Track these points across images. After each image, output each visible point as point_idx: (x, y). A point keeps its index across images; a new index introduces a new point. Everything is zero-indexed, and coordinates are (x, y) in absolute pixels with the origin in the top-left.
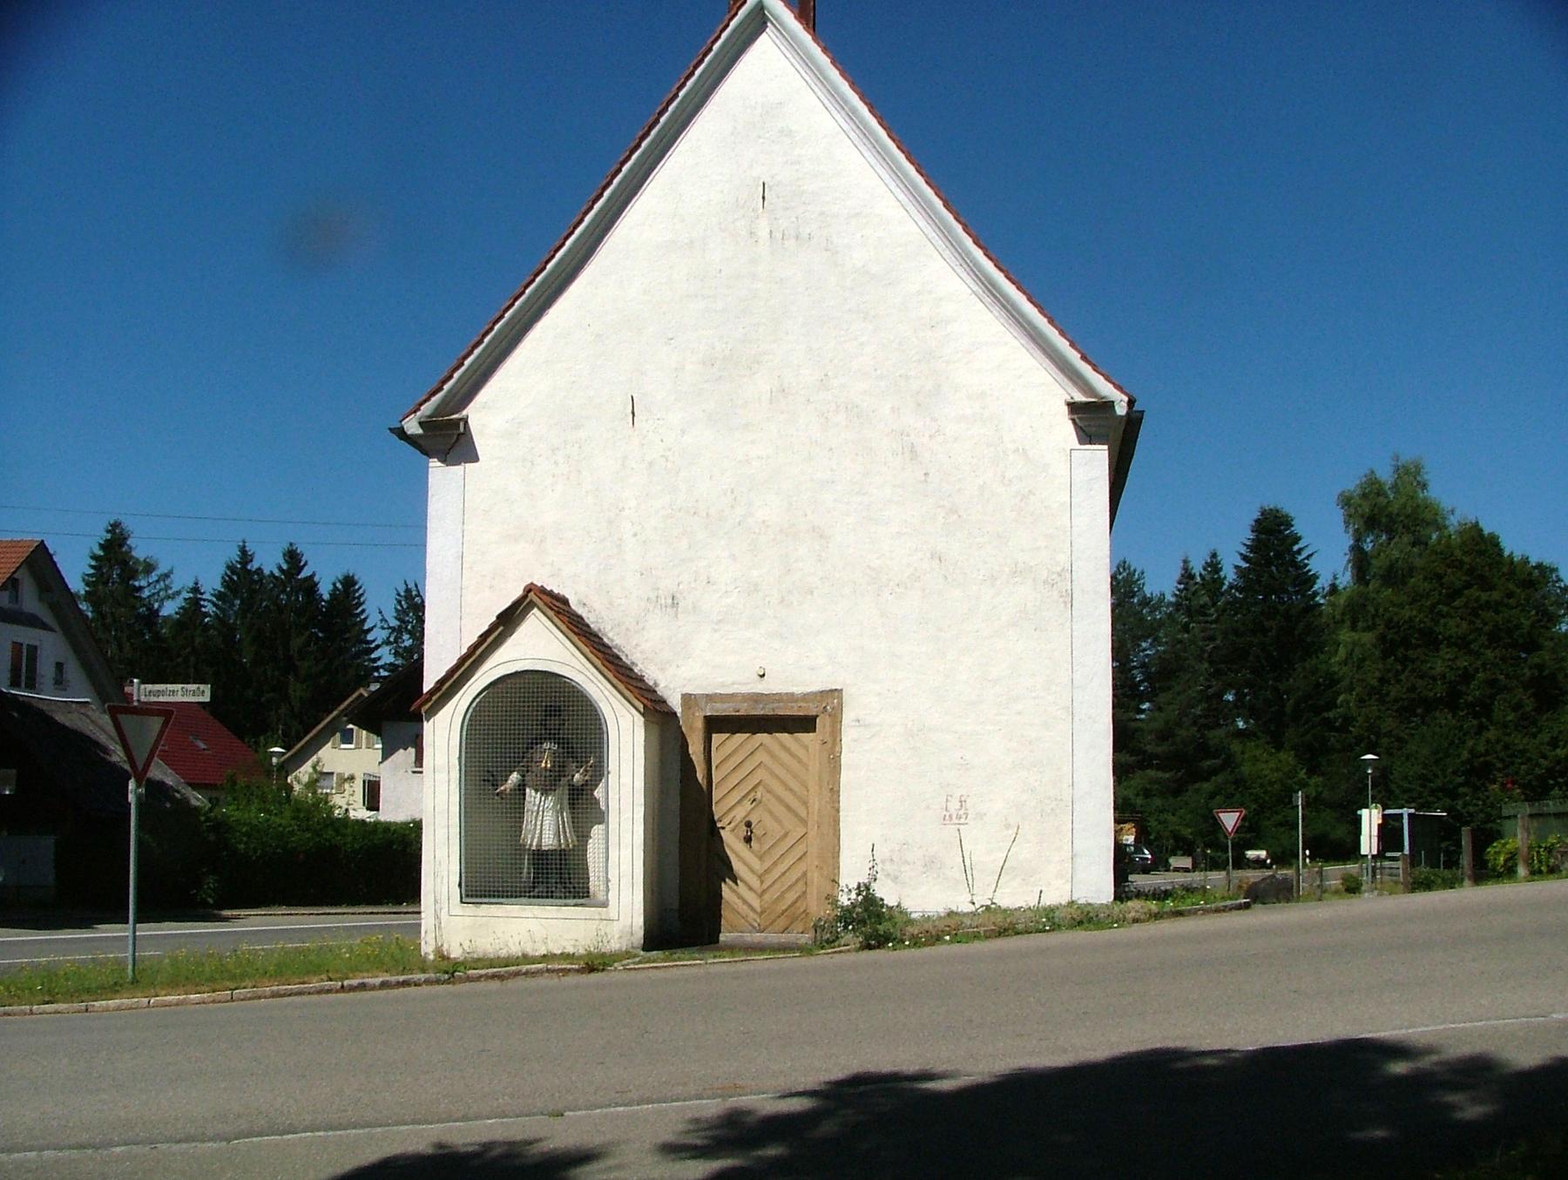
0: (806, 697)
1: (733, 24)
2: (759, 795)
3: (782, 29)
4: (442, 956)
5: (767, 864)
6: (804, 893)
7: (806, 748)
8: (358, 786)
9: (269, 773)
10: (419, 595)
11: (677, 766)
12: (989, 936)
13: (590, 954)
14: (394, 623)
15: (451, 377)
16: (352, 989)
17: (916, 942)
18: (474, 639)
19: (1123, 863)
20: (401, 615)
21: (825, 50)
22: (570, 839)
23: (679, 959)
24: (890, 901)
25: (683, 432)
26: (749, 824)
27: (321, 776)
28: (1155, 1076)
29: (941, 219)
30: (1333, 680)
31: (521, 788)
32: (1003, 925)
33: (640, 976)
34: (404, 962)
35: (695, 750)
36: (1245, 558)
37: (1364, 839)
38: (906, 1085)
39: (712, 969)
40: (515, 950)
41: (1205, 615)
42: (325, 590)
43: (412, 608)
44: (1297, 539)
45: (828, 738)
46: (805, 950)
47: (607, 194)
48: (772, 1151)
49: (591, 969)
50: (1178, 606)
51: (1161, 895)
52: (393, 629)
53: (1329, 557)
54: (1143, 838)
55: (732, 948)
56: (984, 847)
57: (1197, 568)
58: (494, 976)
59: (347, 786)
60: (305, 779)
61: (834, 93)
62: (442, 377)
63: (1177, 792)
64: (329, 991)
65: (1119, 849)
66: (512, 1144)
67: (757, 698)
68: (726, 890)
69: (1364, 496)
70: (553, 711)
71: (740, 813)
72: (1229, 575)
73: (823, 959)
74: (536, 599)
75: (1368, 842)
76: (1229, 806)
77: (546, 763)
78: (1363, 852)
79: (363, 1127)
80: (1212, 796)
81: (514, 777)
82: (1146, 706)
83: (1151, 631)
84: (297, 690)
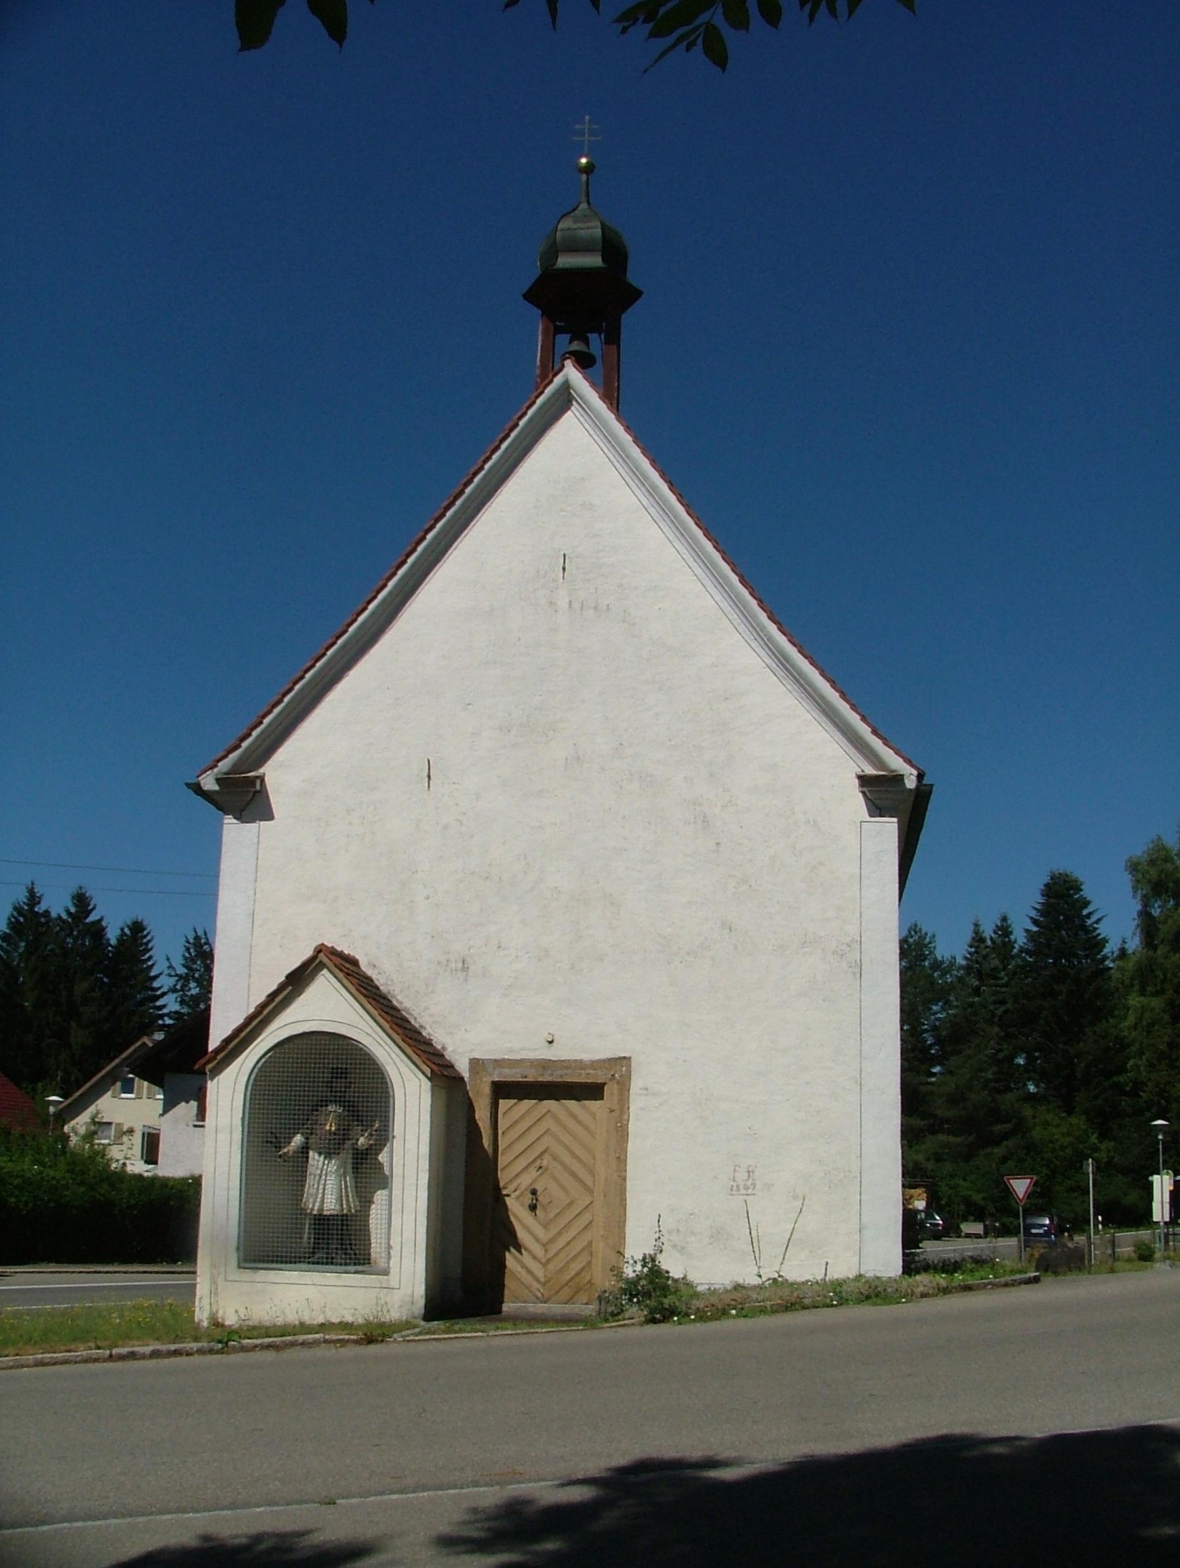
0: (595, 1064)
1: (539, 401)
2: (545, 1163)
3: (586, 408)
4: (216, 1324)
5: (554, 1232)
6: (589, 1263)
7: (593, 1115)
8: (137, 1139)
9: (45, 1124)
10: (207, 943)
11: (461, 1141)
12: (775, 1310)
13: (368, 1323)
14: (182, 971)
15: (249, 735)
16: (122, 1358)
17: (702, 1317)
18: (261, 998)
19: (913, 1230)
20: (188, 963)
21: (628, 429)
22: (352, 1204)
23: (461, 1331)
24: (676, 1273)
25: (478, 796)
26: (534, 1192)
27: (97, 1126)
28: (941, 1470)
29: (737, 595)
30: (1123, 1045)
31: (304, 1150)
32: (790, 1299)
33: (421, 1347)
34: (175, 1329)
35: (482, 1115)
36: (1035, 922)
37: (1156, 1206)
38: (689, 1472)
39: (496, 1342)
40: (292, 1318)
41: (996, 978)
42: (112, 935)
43: (201, 956)
44: (1086, 903)
45: (615, 1106)
46: (587, 1323)
47: (410, 560)
48: (551, 1545)
49: (370, 1340)
50: (968, 969)
51: (949, 1267)
52: (180, 977)
53: (1117, 921)
54: (934, 1203)
55: (516, 1319)
56: (772, 1220)
57: (988, 931)
58: (269, 1346)
59: (125, 1139)
60: (82, 1130)
61: (635, 470)
62: (240, 734)
63: (969, 1157)
64: (96, 1360)
65: (909, 1216)
66: (282, 1536)
67: (545, 1064)
68: (510, 1259)
69: (1152, 862)
70: (340, 1073)
71: (525, 1181)
72: (1020, 938)
73: (607, 1333)
74: (326, 960)
75: (1160, 1209)
76: (1020, 1173)
77: (331, 1126)
78: (1155, 1220)
79: (123, 1516)
80: (1004, 1160)
81: (298, 1139)
82: (936, 1069)
83: (941, 994)
84: (78, 1037)
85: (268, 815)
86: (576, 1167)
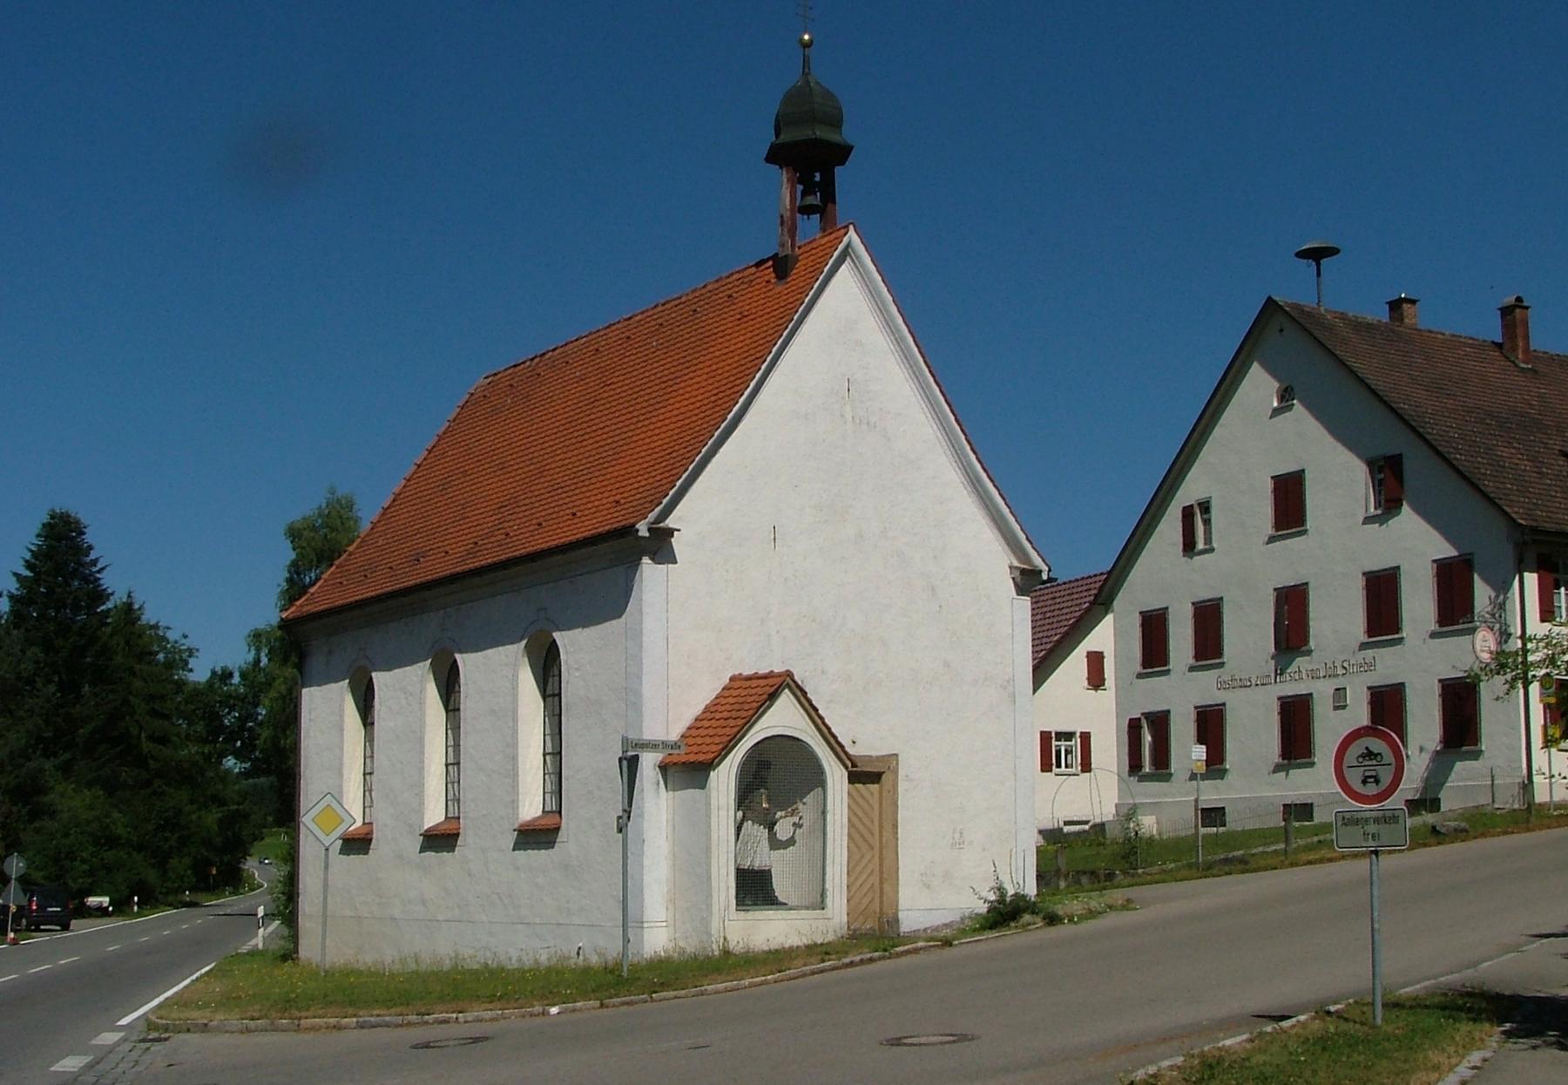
36: (29, 566)
44: (90, 548)
85: (673, 560)
86: (864, 831)
